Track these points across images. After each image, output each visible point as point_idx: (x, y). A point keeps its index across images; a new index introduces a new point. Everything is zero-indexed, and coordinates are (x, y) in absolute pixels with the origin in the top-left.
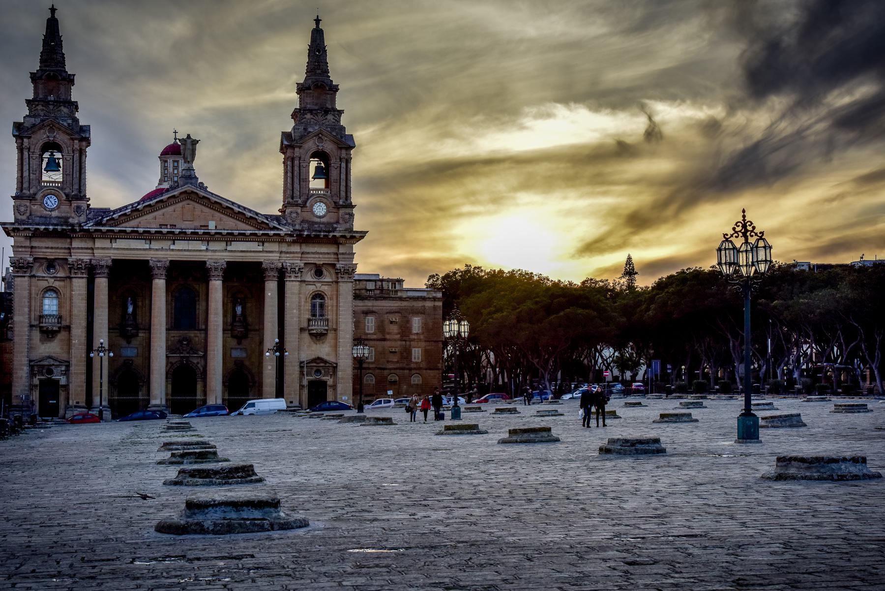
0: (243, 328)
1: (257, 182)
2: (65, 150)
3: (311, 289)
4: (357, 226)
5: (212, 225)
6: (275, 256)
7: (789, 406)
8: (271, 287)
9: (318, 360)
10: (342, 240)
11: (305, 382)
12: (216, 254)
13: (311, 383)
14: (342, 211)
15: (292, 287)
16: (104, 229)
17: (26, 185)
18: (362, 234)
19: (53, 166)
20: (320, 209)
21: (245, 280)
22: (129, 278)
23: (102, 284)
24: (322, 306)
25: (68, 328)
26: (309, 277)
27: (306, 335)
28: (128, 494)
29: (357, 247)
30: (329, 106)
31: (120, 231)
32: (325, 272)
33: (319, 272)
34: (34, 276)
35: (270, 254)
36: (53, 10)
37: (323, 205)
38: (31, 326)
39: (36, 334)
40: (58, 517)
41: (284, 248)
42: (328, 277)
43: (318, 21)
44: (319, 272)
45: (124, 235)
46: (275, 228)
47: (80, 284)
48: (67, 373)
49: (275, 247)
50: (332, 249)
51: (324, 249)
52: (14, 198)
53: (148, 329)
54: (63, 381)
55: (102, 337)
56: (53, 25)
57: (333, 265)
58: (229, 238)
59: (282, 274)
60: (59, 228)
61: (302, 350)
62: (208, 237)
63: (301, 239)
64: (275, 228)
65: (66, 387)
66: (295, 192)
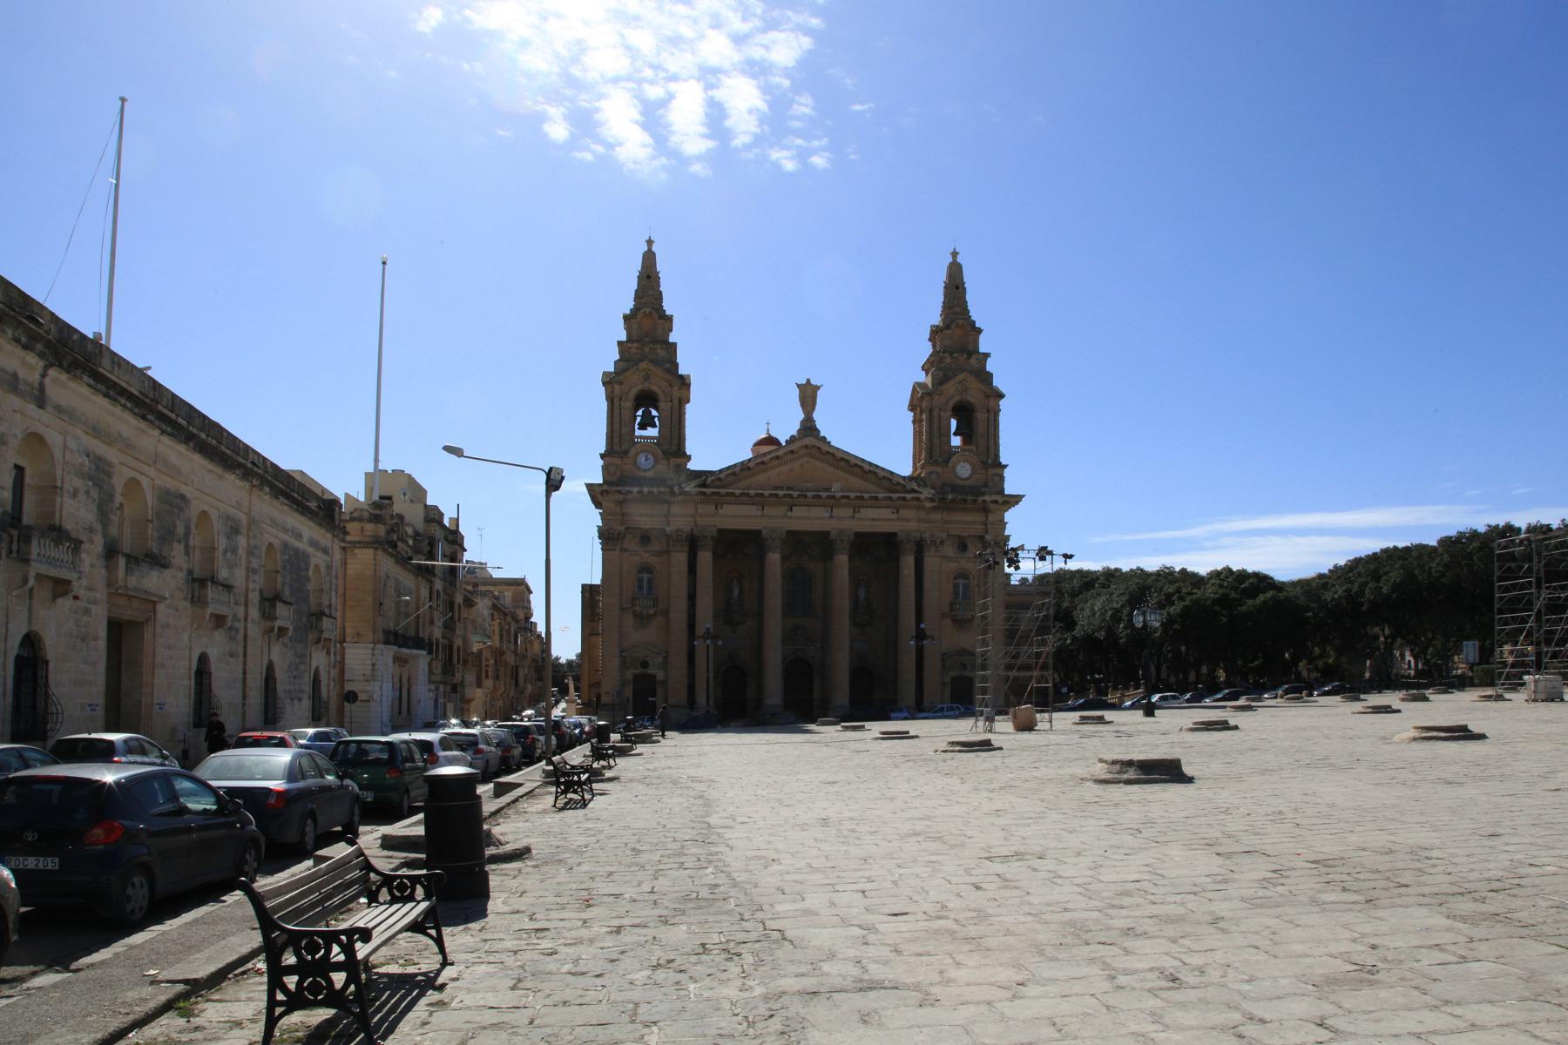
0: (875, 613)
1: (890, 445)
2: (662, 405)
3: (954, 565)
4: (1009, 489)
5: (836, 487)
6: (912, 526)
7: (209, 960)
8: (908, 563)
9: (964, 652)
10: (993, 506)
11: (948, 679)
12: (843, 522)
13: (954, 679)
14: (991, 471)
15: (931, 562)
16: (708, 491)
17: (616, 440)
18: (1017, 499)
19: (647, 422)
20: (964, 470)
21: (878, 551)
22: (739, 547)
23: (705, 558)
24: (966, 587)
25: (666, 613)
26: (949, 550)
27: (948, 622)
28: (871, 1000)
29: (1010, 516)
30: (971, 348)
31: (728, 494)
32: (970, 547)
33: (962, 546)
34: (625, 550)
35: (905, 523)
36: (650, 242)
37: (968, 466)
38: (623, 609)
39: (629, 620)
40: (993, 886)
41: (923, 515)
42: (974, 550)
43: (955, 254)
44: (962, 546)
45: (734, 499)
46: (913, 491)
47: (680, 559)
48: (665, 665)
49: (912, 514)
50: (979, 517)
51: (970, 517)
52: (602, 456)
53: (760, 615)
54: (660, 675)
55: (705, 621)
56: (649, 259)
57: (982, 538)
58: (859, 503)
59: (920, 548)
60: (655, 490)
61: (945, 638)
62: (833, 502)
63: (943, 505)
64: (913, 491)
65: (664, 683)
66: (930, 446)
